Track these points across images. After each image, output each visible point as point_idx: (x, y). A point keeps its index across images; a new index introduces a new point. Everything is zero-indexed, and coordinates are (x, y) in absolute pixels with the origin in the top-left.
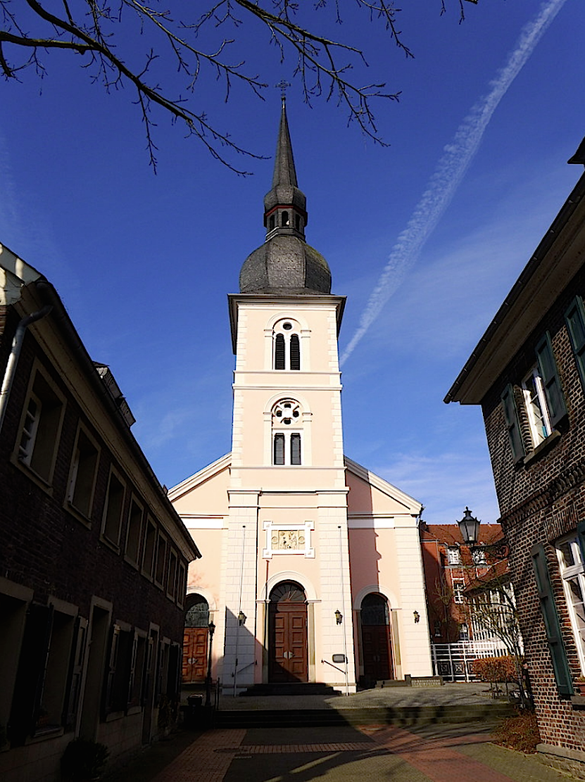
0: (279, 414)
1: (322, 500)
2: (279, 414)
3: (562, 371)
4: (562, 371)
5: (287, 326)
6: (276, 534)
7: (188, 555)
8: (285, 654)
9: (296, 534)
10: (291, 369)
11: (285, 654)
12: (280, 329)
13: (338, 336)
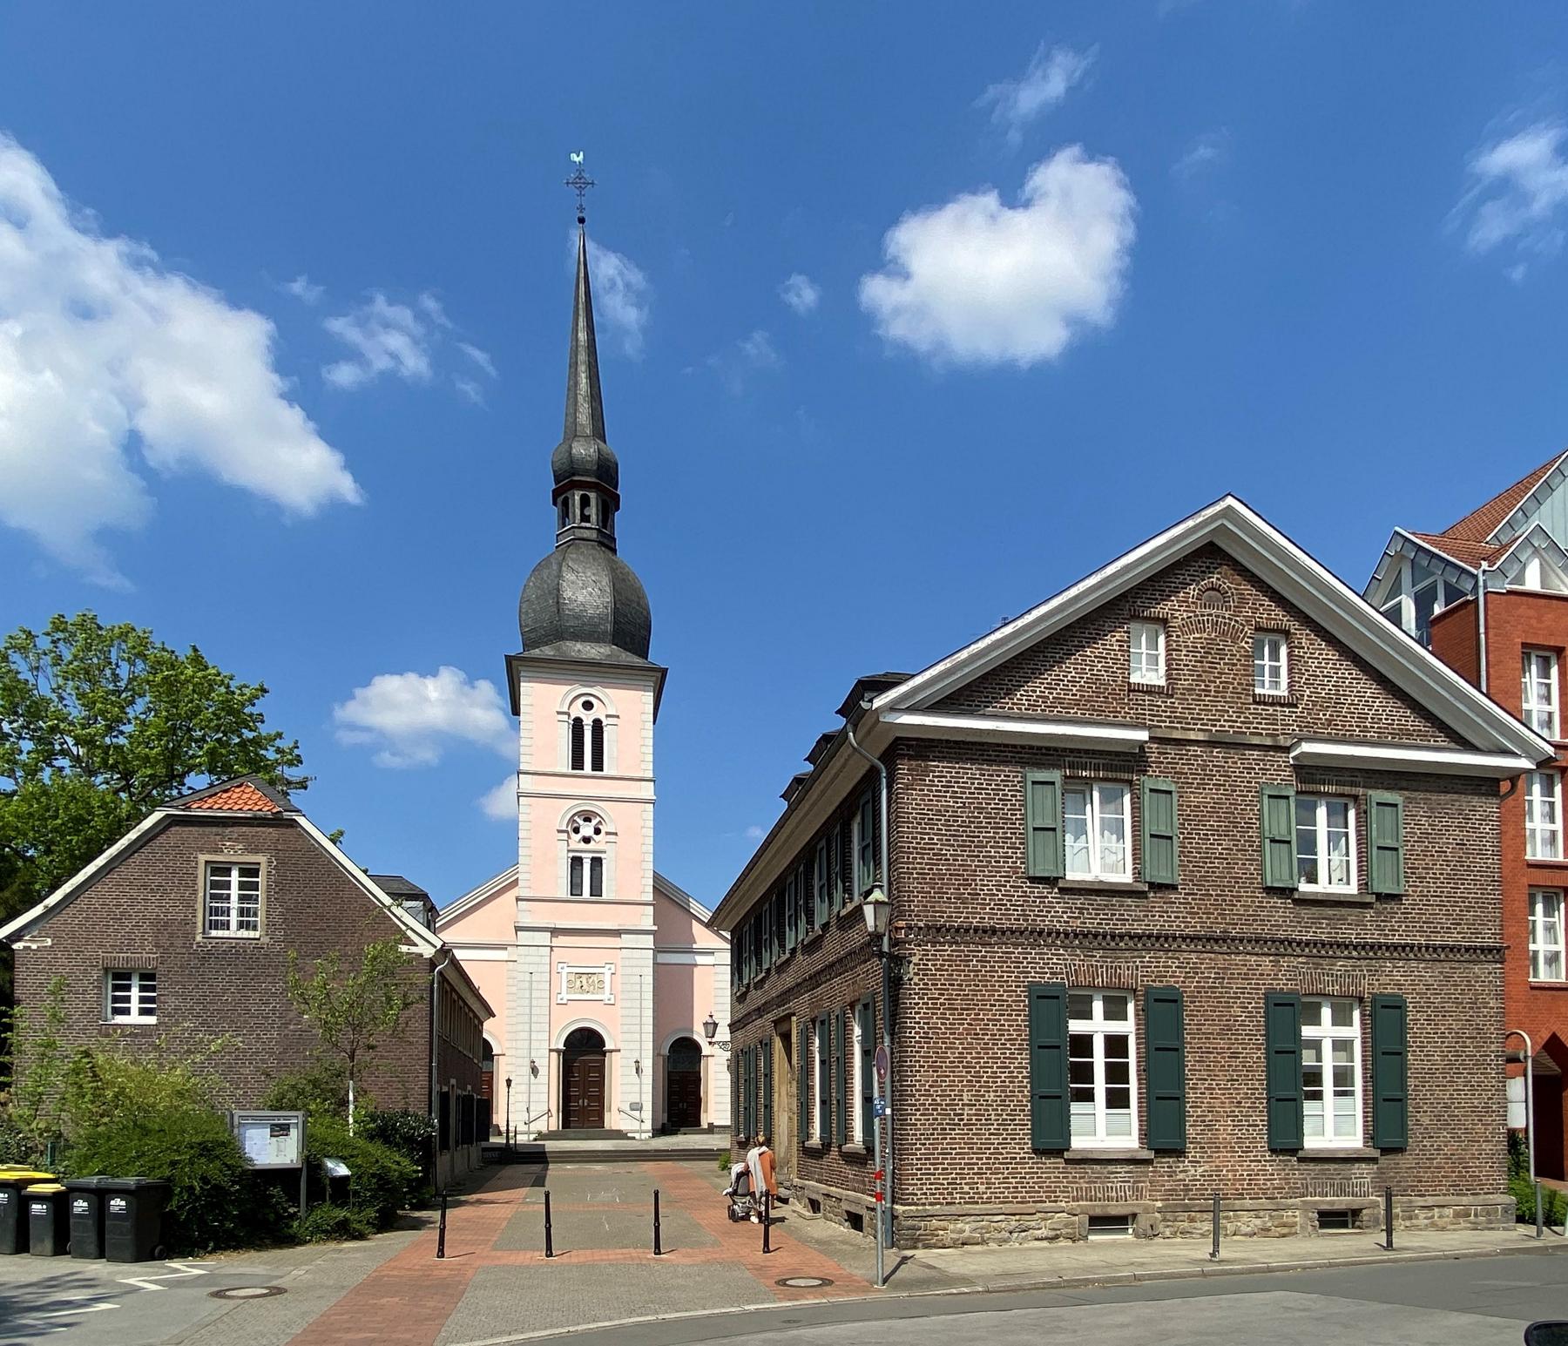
0: (576, 830)
1: (626, 940)
2: (576, 830)
3: (148, 733)
4: (148, 733)
5: (588, 706)
6: (572, 977)
7: (481, 1014)
8: (581, 1101)
9: (594, 978)
10: (573, 769)
11: (581, 1101)
12: (578, 711)
13: (654, 723)
